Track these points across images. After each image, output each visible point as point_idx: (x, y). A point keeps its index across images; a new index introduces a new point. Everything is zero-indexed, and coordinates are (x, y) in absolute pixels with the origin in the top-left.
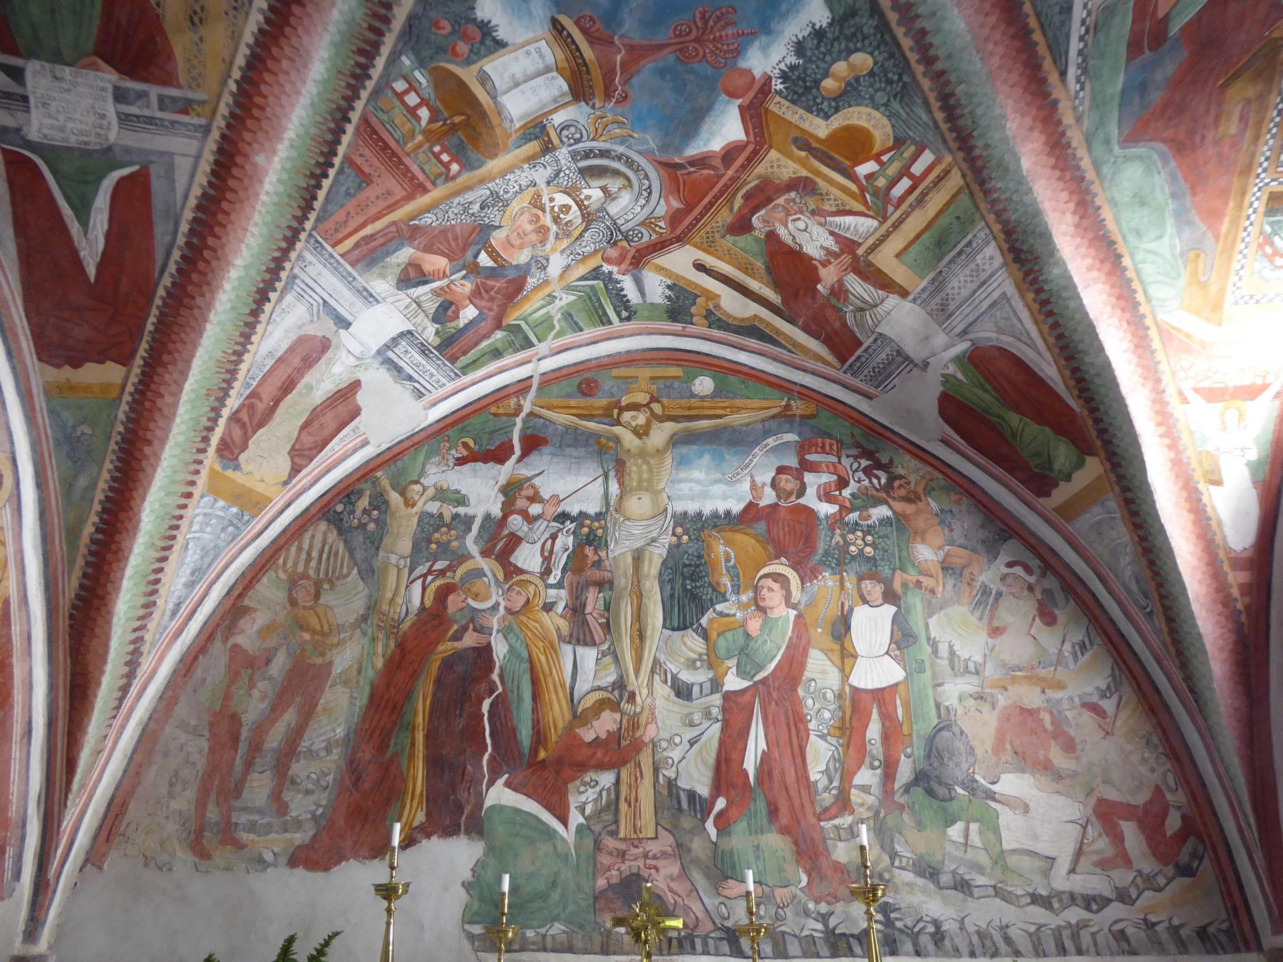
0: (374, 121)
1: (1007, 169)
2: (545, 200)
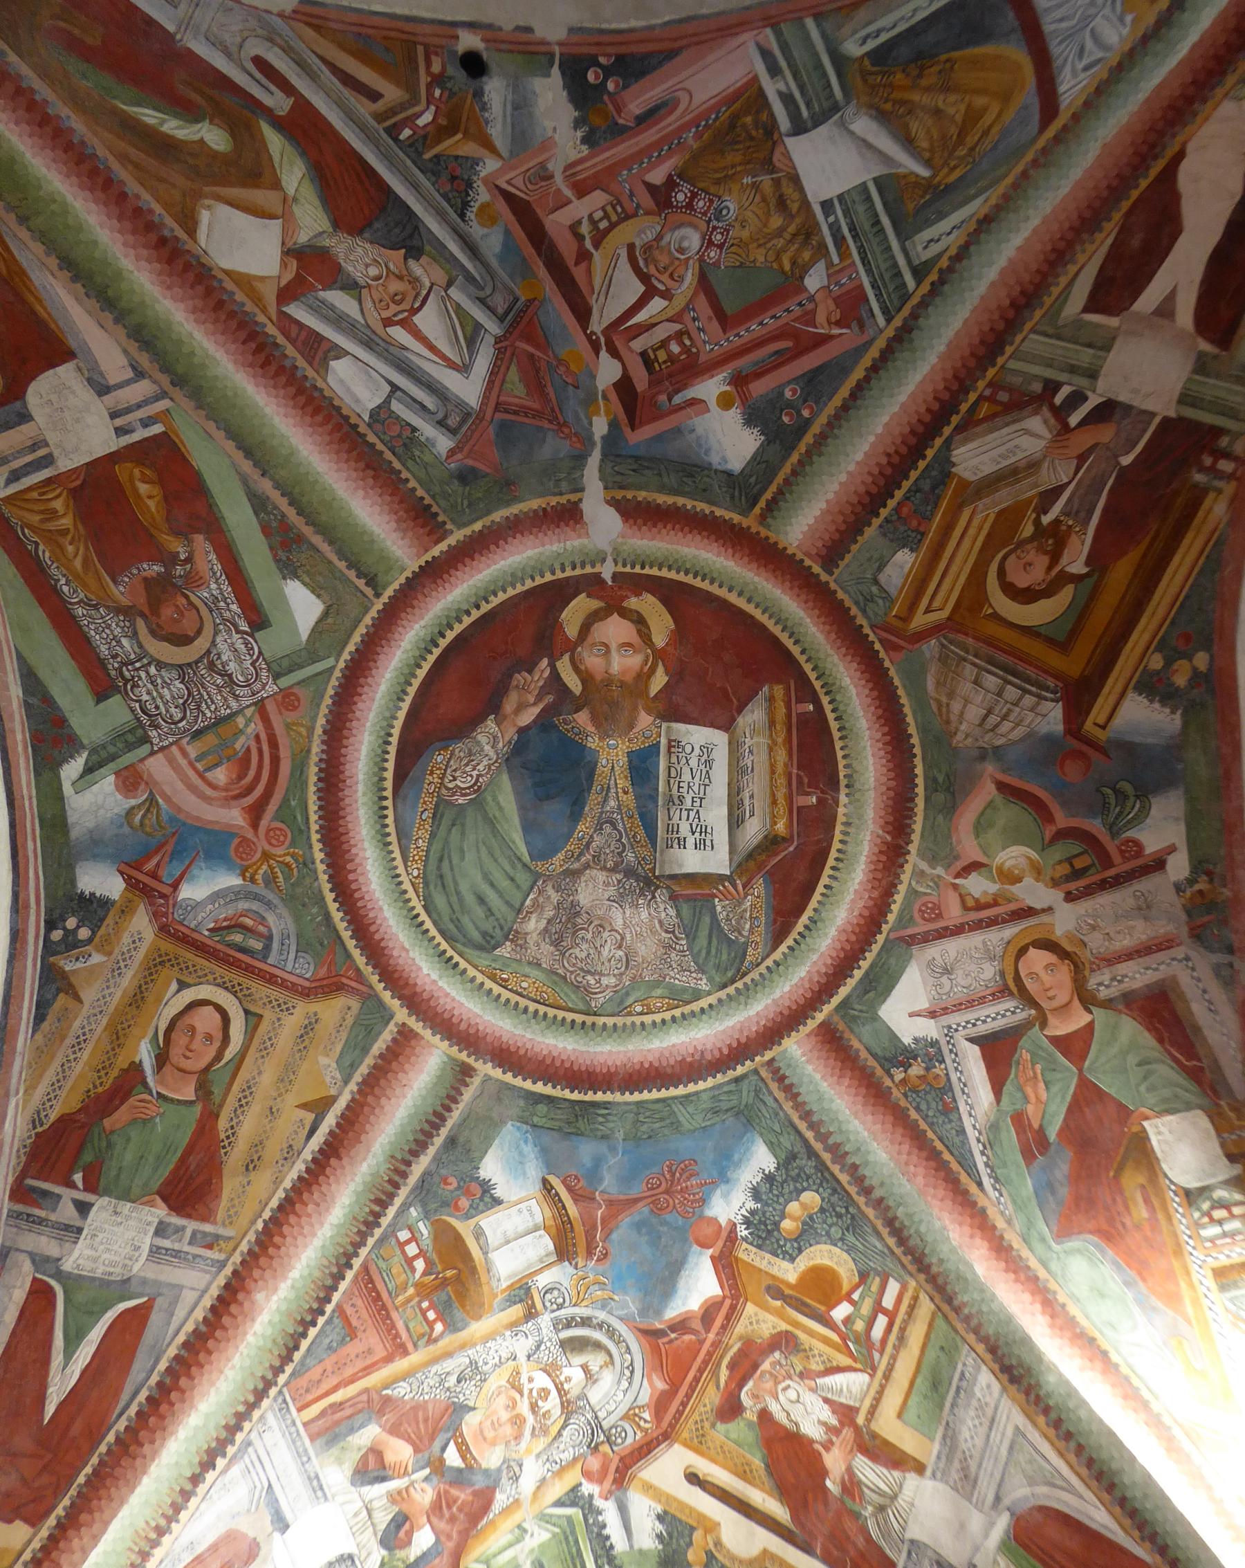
0: (373, 1269)
1: (966, 1280)
2: (524, 1380)
